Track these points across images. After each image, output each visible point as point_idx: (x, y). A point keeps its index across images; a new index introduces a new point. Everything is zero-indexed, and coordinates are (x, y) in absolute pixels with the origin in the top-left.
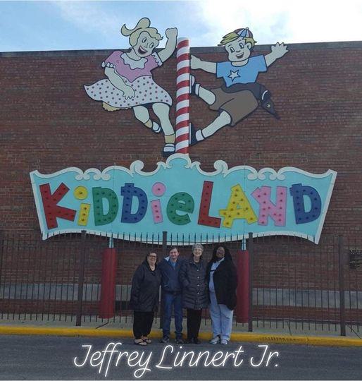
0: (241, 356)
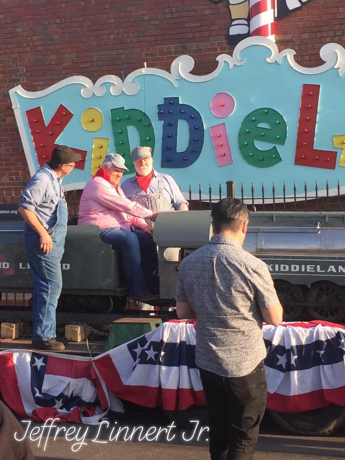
0: (173, 431)
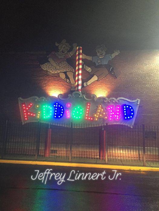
0: (105, 175)
